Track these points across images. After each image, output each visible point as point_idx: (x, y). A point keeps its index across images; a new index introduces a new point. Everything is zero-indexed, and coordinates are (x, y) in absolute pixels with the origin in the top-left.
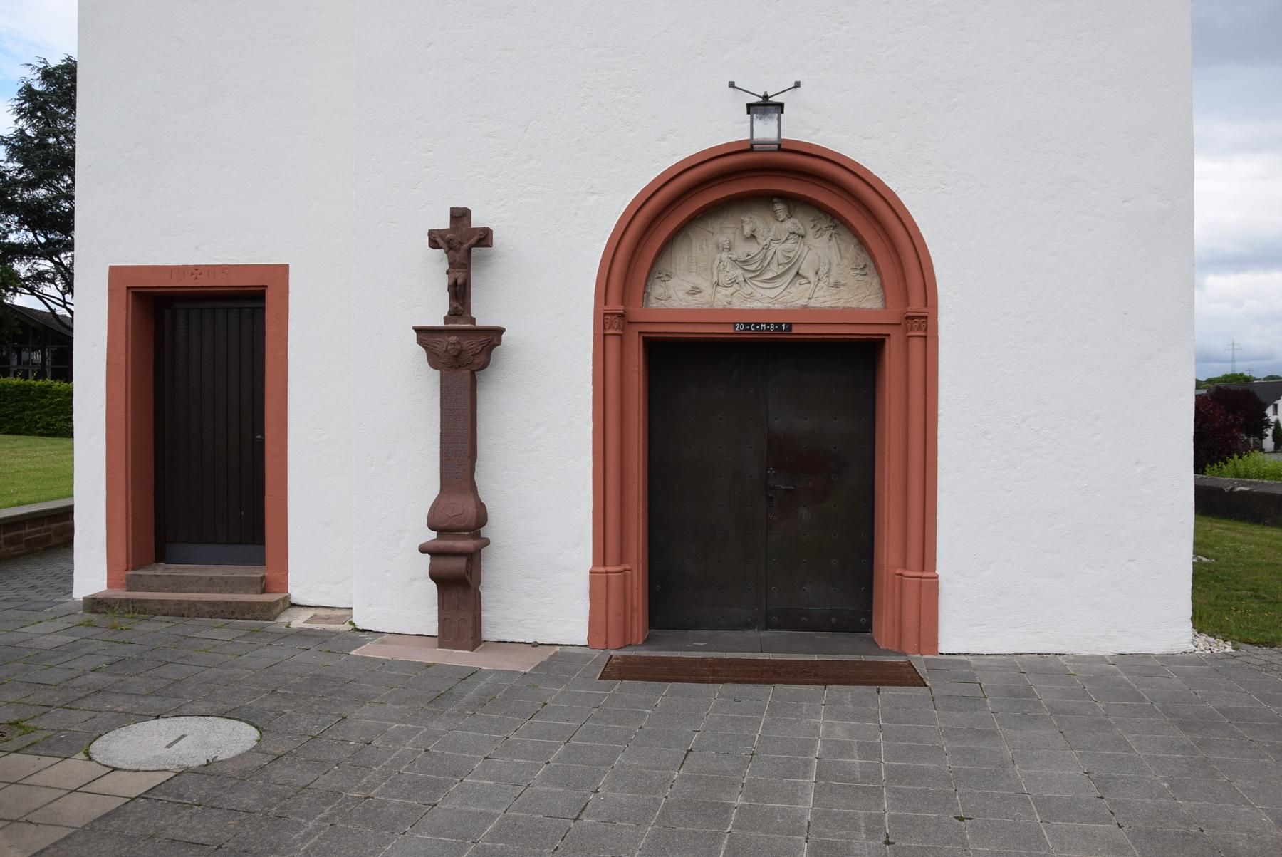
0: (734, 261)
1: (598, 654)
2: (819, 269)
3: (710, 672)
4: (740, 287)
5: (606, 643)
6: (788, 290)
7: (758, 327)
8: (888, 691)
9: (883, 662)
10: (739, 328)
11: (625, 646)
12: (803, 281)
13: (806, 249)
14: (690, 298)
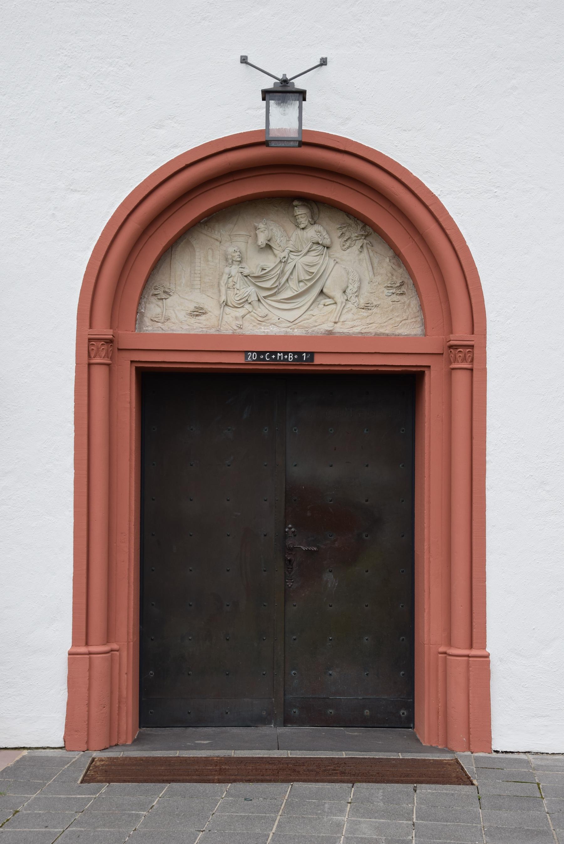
0: (246, 276)
1: (77, 757)
2: (348, 287)
3: (216, 771)
4: (253, 307)
5: (87, 742)
6: (309, 313)
7: (274, 356)
8: (425, 790)
9: (425, 760)
10: (251, 357)
11: (111, 747)
12: (328, 301)
13: (332, 263)
14: (193, 320)
